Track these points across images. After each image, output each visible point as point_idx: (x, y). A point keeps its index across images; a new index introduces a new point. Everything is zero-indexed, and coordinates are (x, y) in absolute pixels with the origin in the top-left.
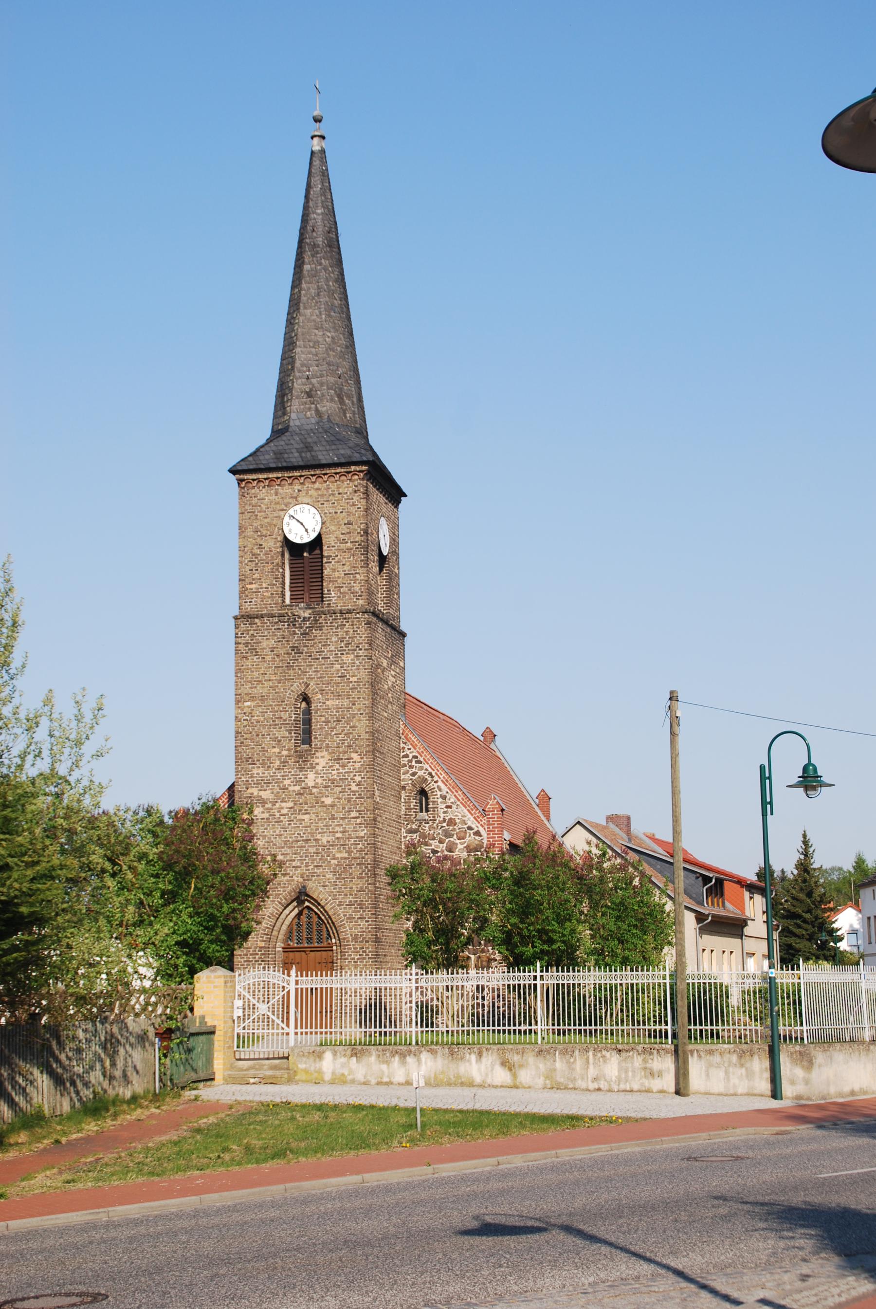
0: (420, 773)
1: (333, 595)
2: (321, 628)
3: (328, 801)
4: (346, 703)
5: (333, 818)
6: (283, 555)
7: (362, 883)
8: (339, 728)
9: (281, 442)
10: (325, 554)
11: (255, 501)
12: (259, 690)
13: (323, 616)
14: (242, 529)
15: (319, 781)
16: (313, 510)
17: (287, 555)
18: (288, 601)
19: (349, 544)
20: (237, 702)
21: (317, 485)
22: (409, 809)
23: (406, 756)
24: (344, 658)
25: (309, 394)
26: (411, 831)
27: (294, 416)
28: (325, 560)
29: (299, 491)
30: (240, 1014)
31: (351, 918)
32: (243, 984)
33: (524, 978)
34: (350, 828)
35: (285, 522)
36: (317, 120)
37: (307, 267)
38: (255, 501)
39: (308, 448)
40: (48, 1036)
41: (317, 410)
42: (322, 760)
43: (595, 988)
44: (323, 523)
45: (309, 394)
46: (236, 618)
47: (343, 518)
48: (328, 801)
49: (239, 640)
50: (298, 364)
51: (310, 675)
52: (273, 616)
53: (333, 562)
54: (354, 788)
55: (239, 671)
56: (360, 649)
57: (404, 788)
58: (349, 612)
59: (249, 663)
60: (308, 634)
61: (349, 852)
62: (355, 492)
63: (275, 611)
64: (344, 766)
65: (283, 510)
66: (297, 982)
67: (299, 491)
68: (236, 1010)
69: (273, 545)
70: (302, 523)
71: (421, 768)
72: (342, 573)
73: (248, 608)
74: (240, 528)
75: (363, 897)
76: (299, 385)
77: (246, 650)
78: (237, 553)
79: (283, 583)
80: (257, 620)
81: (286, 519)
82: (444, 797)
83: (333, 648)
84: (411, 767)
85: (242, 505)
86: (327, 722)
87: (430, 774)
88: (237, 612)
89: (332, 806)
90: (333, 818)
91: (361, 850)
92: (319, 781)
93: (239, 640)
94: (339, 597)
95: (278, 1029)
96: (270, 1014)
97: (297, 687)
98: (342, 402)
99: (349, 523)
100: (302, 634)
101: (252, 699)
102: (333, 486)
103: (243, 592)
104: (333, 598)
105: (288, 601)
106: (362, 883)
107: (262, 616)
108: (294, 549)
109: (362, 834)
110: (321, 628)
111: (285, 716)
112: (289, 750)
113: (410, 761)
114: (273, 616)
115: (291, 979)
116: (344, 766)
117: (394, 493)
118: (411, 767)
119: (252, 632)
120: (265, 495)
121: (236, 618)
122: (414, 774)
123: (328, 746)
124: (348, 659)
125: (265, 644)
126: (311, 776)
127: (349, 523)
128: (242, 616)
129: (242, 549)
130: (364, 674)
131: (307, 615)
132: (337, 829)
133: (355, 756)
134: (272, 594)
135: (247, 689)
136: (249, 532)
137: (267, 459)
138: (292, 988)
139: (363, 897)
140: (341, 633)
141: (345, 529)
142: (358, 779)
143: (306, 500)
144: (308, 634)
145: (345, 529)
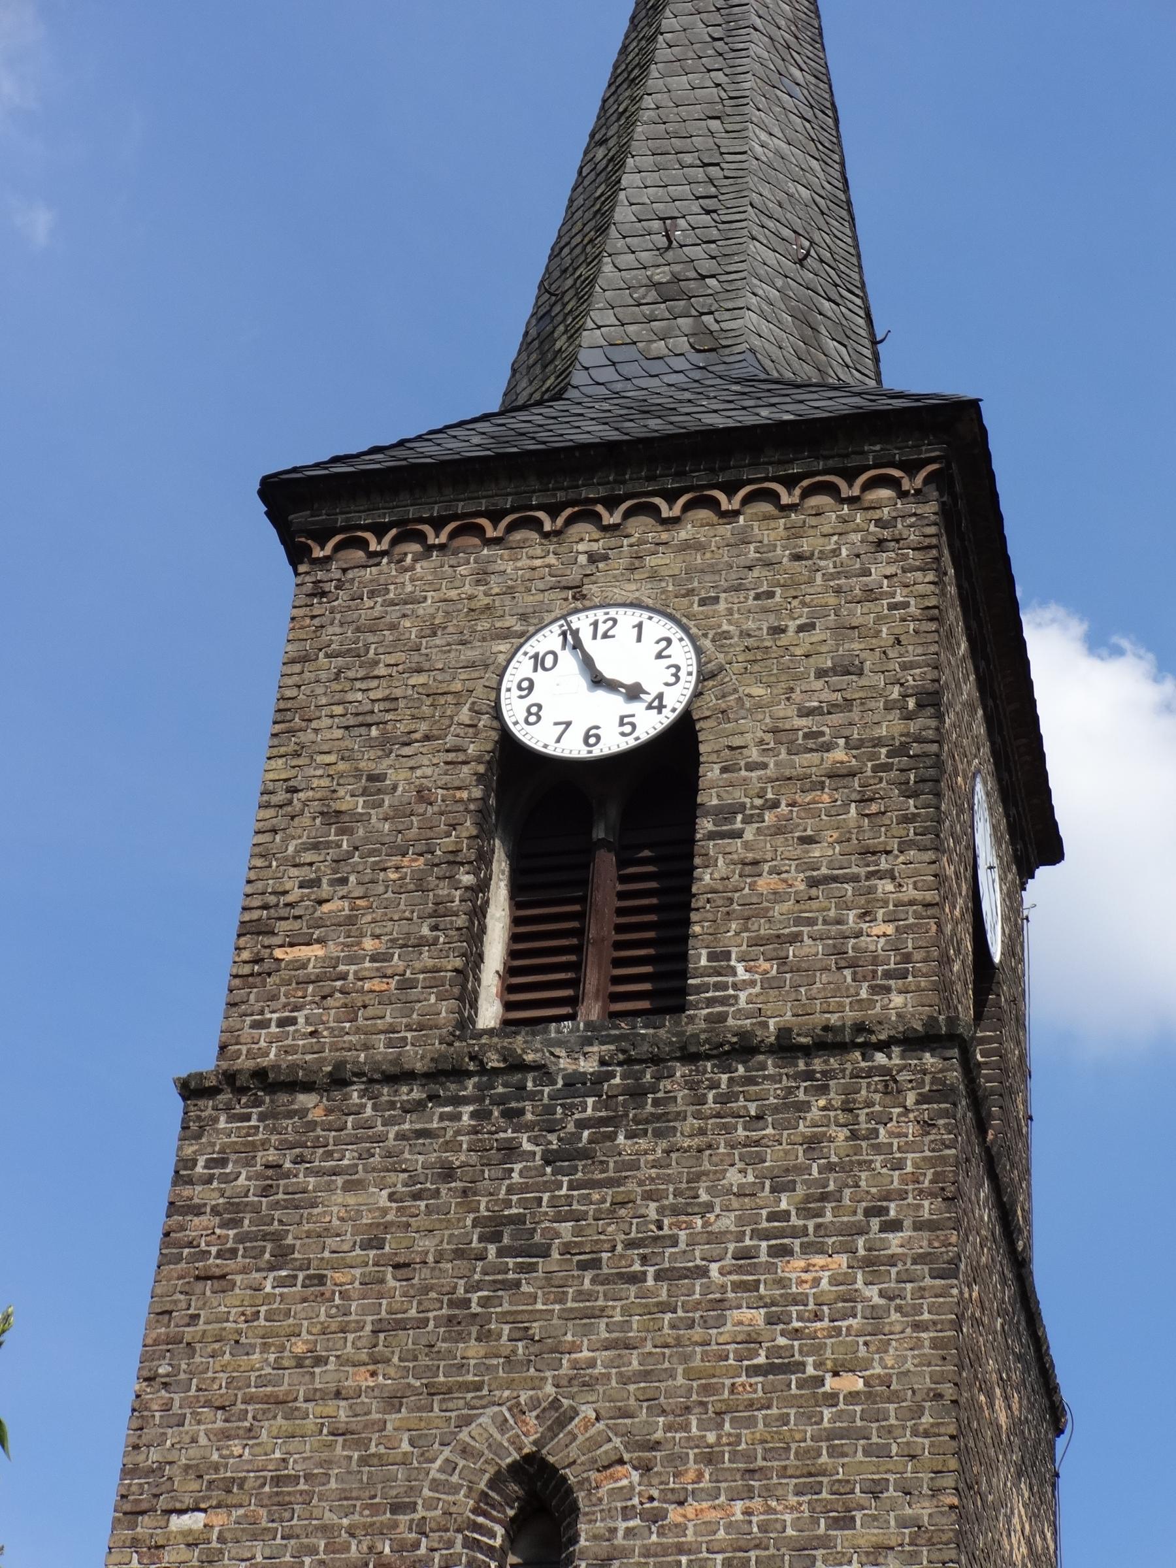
1: (742, 974)
2: (662, 1124)
4: (790, 1514)
6: (484, 859)
10: (709, 798)
11: (372, 608)
12: (272, 1446)
13: (680, 1070)
14: (289, 717)
16: (658, 627)
17: (500, 866)
18: (489, 1013)
19: (839, 754)
20: (130, 1513)
21: (684, 533)
28: (706, 825)
29: (593, 558)
35: (511, 679)
38: (372, 608)
44: (704, 677)
46: (192, 1090)
49: (197, 1193)
51: (588, 1378)
52: (398, 1077)
53: (749, 835)
55: (169, 1345)
56: (894, 1226)
58: (831, 1043)
59: (231, 1305)
60: (585, 1154)
62: (880, 544)
65: (505, 634)
67: (593, 558)
69: (440, 778)
70: (593, 681)
72: (779, 912)
73: (268, 1049)
74: (282, 713)
76: (621, 268)
77: (214, 1245)
79: (475, 935)
80: (305, 1100)
81: (548, 640)
83: (728, 1222)
88: (204, 1061)
93: (197, 1193)
94: (770, 984)
97: (499, 1433)
100: (549, 1158)
101: (221, 1489)
103: (254, 974)
104: (739, 982)
105: (489, 1013)
107: (338, 1080)
108: (536, 799)
110: (662, 1124)
114: (398, 1077)
119: (272, 1156)
120: (419, 584)
121: (192, 1090)
124: (813, 1273)
128: (230, 1078)
129: (281, 799)
130: (906, 1358)
131: (588, 1066)
134: (406, 985)
135: (200, 1436)
136: (327, 731)
141: (822, 693)
143: (630, 590)
144: (585, 1154)
145: (822, 693)
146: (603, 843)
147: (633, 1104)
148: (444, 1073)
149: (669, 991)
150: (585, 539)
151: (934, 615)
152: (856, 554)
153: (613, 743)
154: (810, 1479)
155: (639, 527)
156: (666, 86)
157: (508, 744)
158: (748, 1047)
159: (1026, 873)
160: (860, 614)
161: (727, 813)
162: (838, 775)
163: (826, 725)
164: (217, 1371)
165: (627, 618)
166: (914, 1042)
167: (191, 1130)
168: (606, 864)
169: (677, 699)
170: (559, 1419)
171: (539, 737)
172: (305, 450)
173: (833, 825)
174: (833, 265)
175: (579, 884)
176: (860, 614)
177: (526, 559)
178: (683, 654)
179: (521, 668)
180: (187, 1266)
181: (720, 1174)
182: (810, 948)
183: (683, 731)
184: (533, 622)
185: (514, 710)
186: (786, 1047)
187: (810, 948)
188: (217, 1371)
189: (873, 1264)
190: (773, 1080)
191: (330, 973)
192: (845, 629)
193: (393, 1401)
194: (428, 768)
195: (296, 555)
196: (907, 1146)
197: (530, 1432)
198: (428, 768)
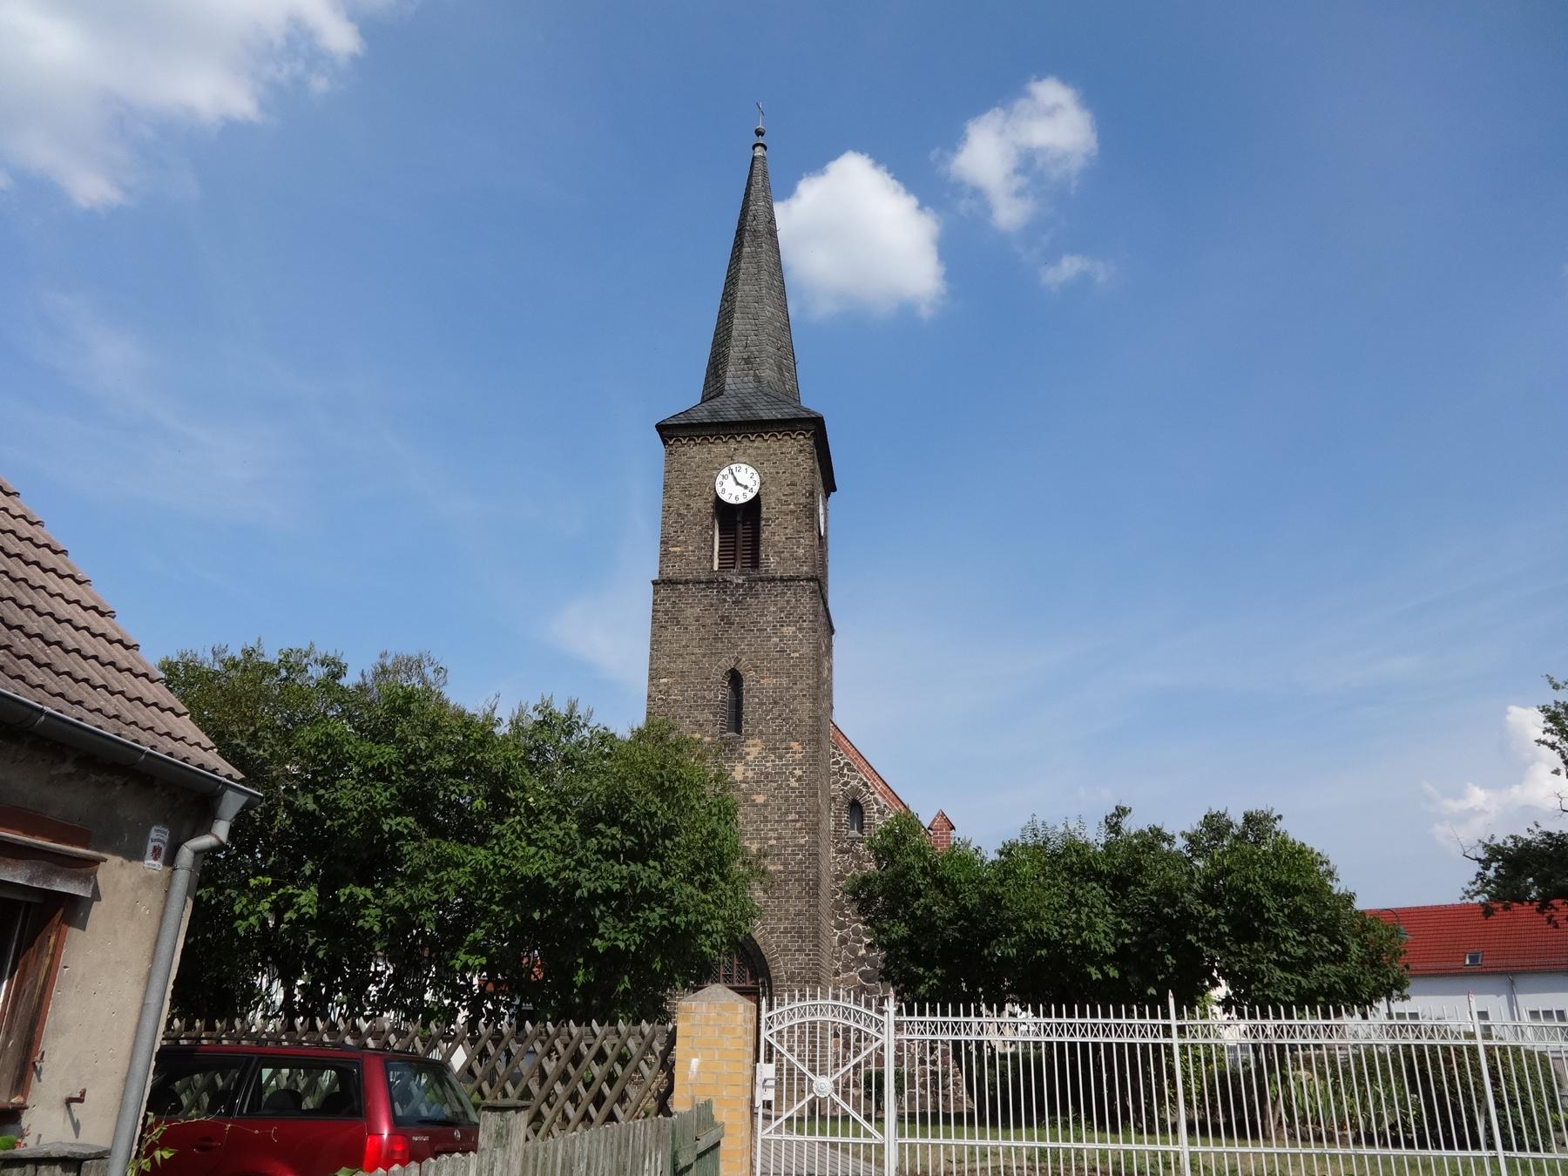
0: (854, 783)
3: (760, 799)
5: (766, 820)
7: (800, 905)
8: (776, 711)
9: (716, 403)
10: (764, 515)
11: (684, 459)
12: (679, 665)
15: (750, 774)
16: (751, 470)
20: (651, 678)
22: (838, 824)
23: (837, 763)
24: (784, 629)
25: (747, 361)
26: (841, 851)
27: (729, 380)
30: (770, 1095)
31: (786, 949)
32: (776, 1028)
33: (1291, 1031)
34: (787, 833)
36: (759, 133)
37: (746, 250)
39: (747, 407)
40: (581, 960)
41: (755, 375)
42: (753, 749)
43: (1357, 1058)
45: (747, 361)
46: (655, 583)
47: (786, 478)
48: (760, 799)
50: (734, 333)
51: (743, 651)
52: (700, 582)
54: (793, 783)
55: (656, 642)
57: (834, 799)
58: (791, 579)
61: (785, 864)
63: (703, 578)
64: (781, 758)
66: (899, 1027)
68: (759, 1090)
69: (703, 506)
70: (737, 483)
71: (855, 778)
73: (670, 573)
74: (665, 486)
75: (804, 923)
76: (735, 352)
77: (664, 619)
78: (660, 513)
79: (712, 546)
81: (725, 471)
82: (881, 812)
84: (843, 775)
85: (669, 463)
86: (761, 704)
87: (865, 784)
89: (765, 805)
90: (766, 820)
91: (801, 862)
92: (750, 774)
95: (856, 1135)
96: (838, 1099)
97: (726, 663)
98: (782, 374)
99: (793, 484)
101: (671, 674)
102: (775, 446)
103: (665, 554)
104: (772, 562)
106: (800, 905)
107: (687, 582)
108: (723, 510)
109: (802, 841)
110: (756, 596)
111: (709, 695)
112: (713, 736)
113: (842, 769)
114: (700, 582)
115: (885, 1019)
116: (781, 758)
117: (830, 486)
118: (843, 775)
120: (695, 452)
121: (655, 583)
122: (846, 784)
123: (761, 732)
124: (788, 631)
125: (689, 612)
126: (740, 768)
127: (793, 484)
129: (667, 509)
130: (807, 650)
132: (771, 834)
133: (794, 745)
137: (703, 416)
138: (889, 1039)
139: (804, 923)
140: (781, 602)
141: (788, 490)
142: (798, 772)
145: (788, 490)
146: (740, 524)
147: (750, 591)
148: (710, 582)
149: (755, 562)
150: (733, 445)
151: (813, 471)
152: (794, 451)
153: (742, 500)
154: (788, 675)
155: (746, 442)
156: (744, 290)
157: (718, 501)
158: (774, 579)
159: (827, 496)
160: (796, 470)
161: (768, 520)
162: (792, 512)
163: (789, 499)
164: (667, 648)
165: (744, 466)
166: (808, 580)
167: (656, 592)
168: (740, 526)
169: (756, 489)
170: (738, 661)
171: (725, 497)
172: (664, 415)
173: (791, 523)
174: (794, 395)
175: (735, 531)
176: (796, 470)
177: (719, 448)
178: (756, 477)
179: (719, 479)
180: (658, 626)
181: (769, 607)
182: (786, 555)
183: (757, 497)
184: (722, 466)
185: (719, 489)
186: (782, 580)
187: (786, 555)
188: (667, 648)
189: (800, 629)
190: (780, 587)
191: (682, 555)
192: (793, 474)
193: (704, 656)
194: (700, 504)
195: (665, 443)
196: (807, 603)
197: (733, 663)
198: (700, 504)
